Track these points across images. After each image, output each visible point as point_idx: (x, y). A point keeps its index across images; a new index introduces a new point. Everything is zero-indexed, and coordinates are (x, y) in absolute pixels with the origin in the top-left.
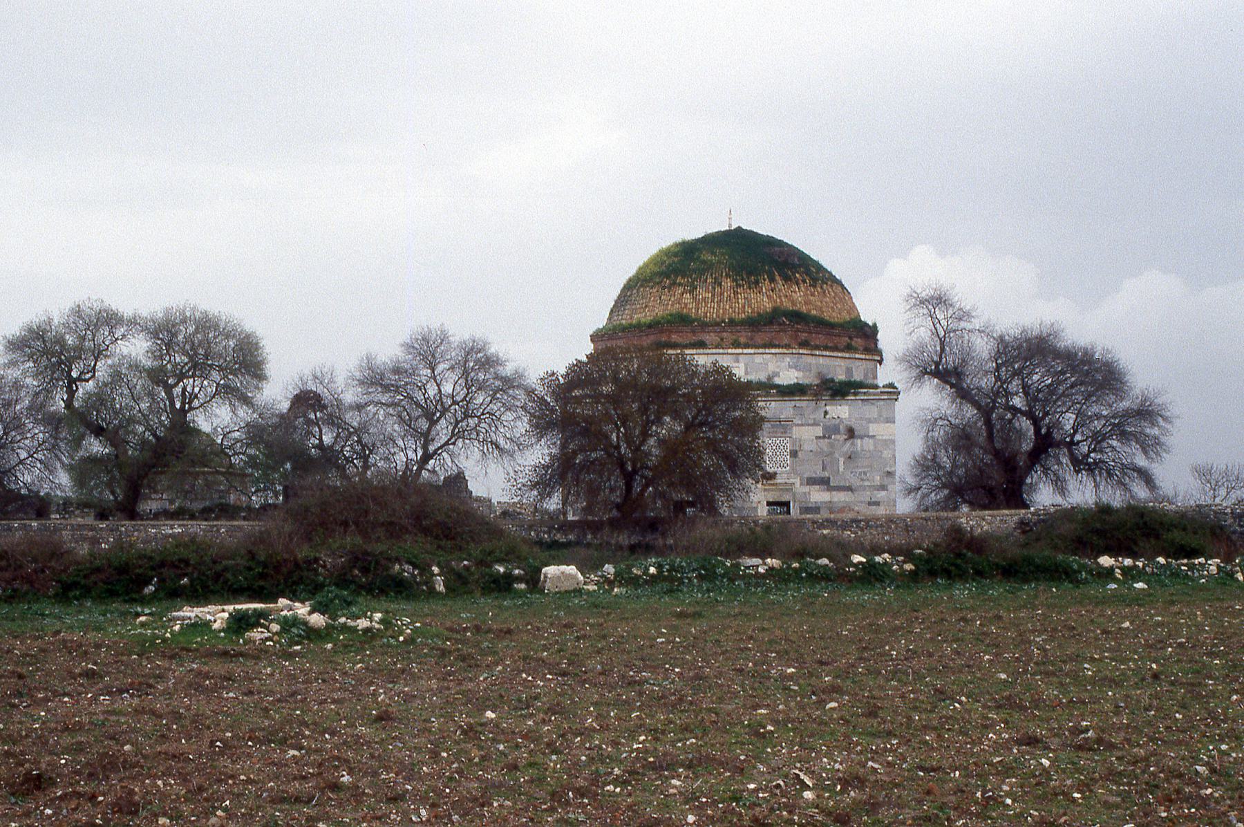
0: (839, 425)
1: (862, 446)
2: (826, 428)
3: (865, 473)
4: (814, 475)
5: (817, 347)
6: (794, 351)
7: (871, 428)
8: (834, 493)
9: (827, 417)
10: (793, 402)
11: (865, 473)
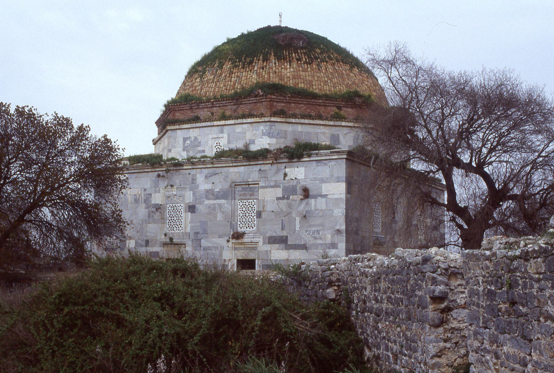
0: (296, 186)
1: (315, 205)
2: (285, 190)
3: (318, 232)
4: (274, 234)
5: (294, 116)
6: (266, 119)
7: (323, 188)
8: (291, 251)
9: (286, 178)
10: (258, 166)
11: (318, 232)
